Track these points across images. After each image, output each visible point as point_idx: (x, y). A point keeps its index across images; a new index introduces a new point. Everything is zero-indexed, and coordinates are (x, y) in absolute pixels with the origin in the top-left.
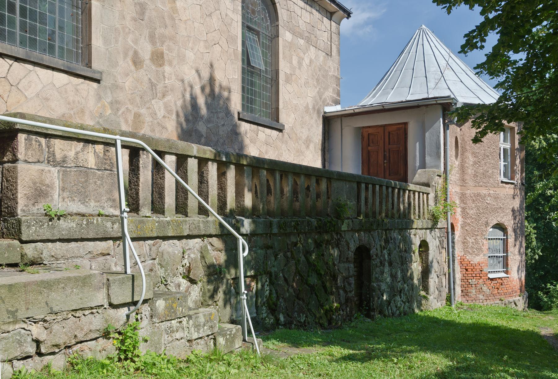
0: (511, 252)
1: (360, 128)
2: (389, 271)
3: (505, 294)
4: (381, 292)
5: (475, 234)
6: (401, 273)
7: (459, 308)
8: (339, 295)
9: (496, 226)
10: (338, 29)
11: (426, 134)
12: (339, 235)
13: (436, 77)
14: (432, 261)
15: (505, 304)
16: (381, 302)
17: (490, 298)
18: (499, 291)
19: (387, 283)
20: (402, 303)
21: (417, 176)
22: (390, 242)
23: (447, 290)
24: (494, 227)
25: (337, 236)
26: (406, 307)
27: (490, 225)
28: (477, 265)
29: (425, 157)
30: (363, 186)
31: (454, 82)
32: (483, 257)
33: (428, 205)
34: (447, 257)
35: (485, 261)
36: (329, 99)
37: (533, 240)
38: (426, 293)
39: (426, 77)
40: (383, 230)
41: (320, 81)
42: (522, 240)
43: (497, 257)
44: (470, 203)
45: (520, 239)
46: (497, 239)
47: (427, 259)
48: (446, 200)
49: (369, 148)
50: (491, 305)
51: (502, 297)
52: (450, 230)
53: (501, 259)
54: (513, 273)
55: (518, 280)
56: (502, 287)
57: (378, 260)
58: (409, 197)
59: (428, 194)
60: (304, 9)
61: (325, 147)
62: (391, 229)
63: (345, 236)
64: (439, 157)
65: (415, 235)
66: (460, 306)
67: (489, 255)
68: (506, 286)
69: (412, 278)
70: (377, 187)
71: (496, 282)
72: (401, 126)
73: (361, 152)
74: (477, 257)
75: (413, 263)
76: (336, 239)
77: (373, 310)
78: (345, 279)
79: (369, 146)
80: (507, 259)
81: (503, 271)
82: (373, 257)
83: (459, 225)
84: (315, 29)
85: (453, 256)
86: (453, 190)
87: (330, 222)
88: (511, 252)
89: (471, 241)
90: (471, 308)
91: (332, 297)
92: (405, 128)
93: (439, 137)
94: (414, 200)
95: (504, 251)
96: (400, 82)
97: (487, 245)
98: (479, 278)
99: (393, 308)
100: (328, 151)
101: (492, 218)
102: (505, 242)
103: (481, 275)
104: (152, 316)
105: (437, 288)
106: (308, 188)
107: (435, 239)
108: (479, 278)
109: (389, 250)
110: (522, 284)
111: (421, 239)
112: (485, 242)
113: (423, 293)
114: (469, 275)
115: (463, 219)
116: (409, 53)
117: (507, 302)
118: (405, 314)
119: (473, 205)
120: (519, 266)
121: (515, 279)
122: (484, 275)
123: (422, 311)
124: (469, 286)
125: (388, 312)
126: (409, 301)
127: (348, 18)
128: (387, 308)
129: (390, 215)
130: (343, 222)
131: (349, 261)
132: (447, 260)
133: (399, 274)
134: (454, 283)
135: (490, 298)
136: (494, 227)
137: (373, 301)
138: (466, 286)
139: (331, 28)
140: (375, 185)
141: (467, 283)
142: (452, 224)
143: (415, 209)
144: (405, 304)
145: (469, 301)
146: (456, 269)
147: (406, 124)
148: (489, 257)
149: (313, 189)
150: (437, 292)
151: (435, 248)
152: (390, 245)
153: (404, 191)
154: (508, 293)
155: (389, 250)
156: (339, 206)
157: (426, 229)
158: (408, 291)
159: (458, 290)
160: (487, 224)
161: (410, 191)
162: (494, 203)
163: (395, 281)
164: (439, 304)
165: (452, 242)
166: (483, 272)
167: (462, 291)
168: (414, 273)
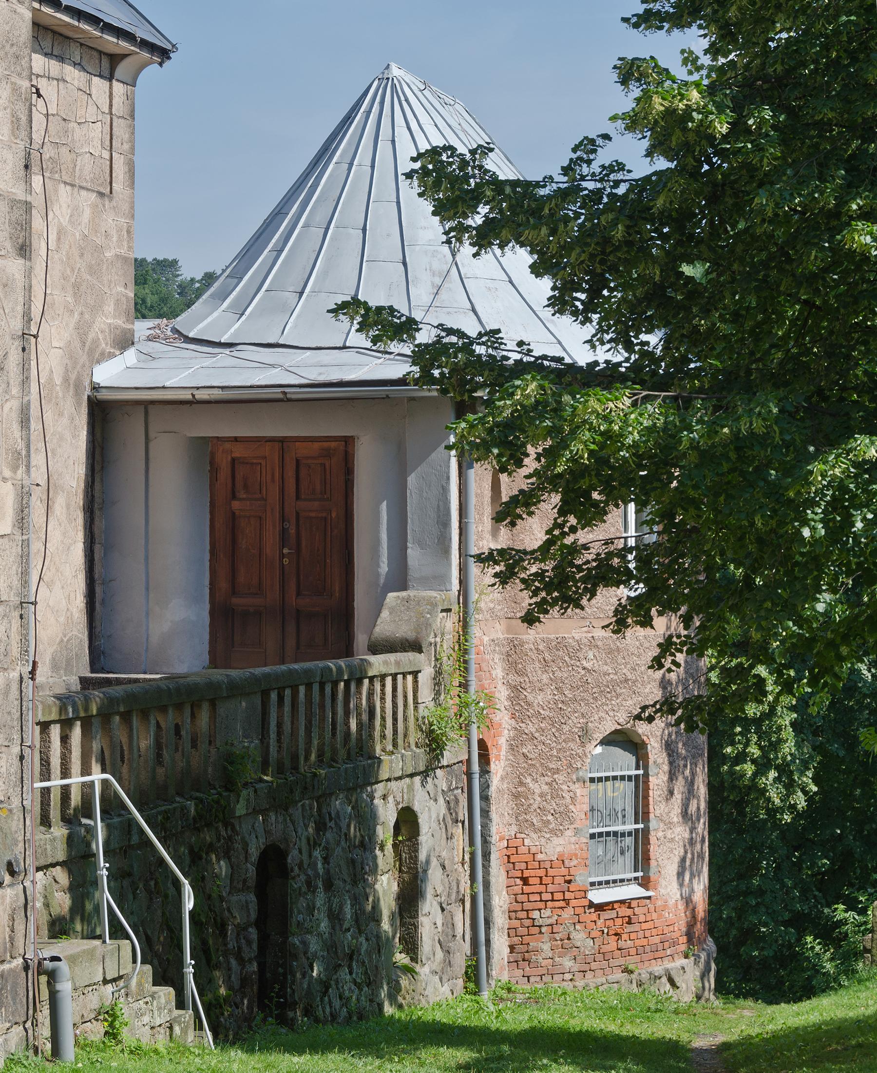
0: (660, 819)
1: (205, 440)
2: (325, 903)
3: (641, 950)
4: (308, 959)
5: (551, 766)
6: (352, 906)
7: (502, 999)
8: (229, 969)
9: (613, 737)
10: (130, 99)
11: (409, 479)
12: (229, 828)
13: (436, 265)
14: (428, 862)
15: (640, 984)
16: (309, 985)
17: (594, 965)
18: (621, 944)
19: (320, 935)
20: (353, 987)
21: (385, 614)
22: (329, 824)
23: (467, 948)
24: (607, 741)
25: (226, 830)
26: (363, 998)
27: (595, 736)
28: (557, 863)
29: (406, 548)
30: (274, 696)
31: (490, 284)
32: (573, 839)
33: (416, 703)
34: (467, 849)
35: (579, 852)
36: (105, 339)
37: (784, 735)
38: (412, 959)
39: (405, 264)
40: (312, 798)
41: (83, 288)
42: (693, 774)
43: (615, 834)
44: (535, 672)
45: (687, 772)
46: (615, 778)
47: (414, 858)
48: (464, 686)
49: (236, 505)
50: (597, 987)
51: (631, 962)
52: (476, 768)
53: (629, 841)
54: (663, 883)
55: (681, 906)
56: (630, 928)
57: (303, 878)
58: (371, 694)
59: (415, 674)
60: (44, 76)
61: (93, 496)
62: (331, 794)
63: (240, 827)
64: (447, 551)
65: (384, 797)
66: (504, 993)
67: (592, 831)
68: (644, 926)
69: (375, 916)
70: (302, 689)
71: (613, 914)
72: (333, 445)
73: (208, 516)
74: (556, 841)
75: (379, 877)
76: (224, 838)
77: (293, 1005)
78: (241, 929)
79: (234, 497)
80: (647, 842)
81: (636, 879)
82: (292, 870)
83: (503, 741)
84: (73, 125)
85: (486, 842)
86: (486, 639)
87: (218, 802)
88: (660, 819)
89: (537, 791)
90: (534, 999)
91: (217, 973)
92: (346, 452)
93: (445, 490)
94: (383, 699)
95: (636, 814)
96: (325, 273)
97: (587, 800)
98: (562, 904)
99: (333, 1001)
100: (101, 509)
101: (603, 715)
102: (641, 785)
103: (568, 895)
104: (127, 995)
105: (439, 941)
106: (177, 729)
107: (436, 800)
108: (562, 904)
109: (326, 848)
110: (694, 917)
111: (400, 807)
112: (579, 792)
113: (401, 958)
114: (533, 898)
115: (513, 722)
116: (351, 164)
117: (645, 976)
118: (361, 1018)
119: (545, 678)
120: (683, 860)
121: (671, 902)
122: (578, 895)
123: (400, 1007)
124: (535, 930)
125: (324, 1011)
126: (371, 982)
127: (161, 64)
128: (322, 1000)
129: (328, 755)
130: (239, 796)
131: (248, 888)
132: (467, 857)
133: (348, 910)
134: (488, 923)
135: (594, 965)
136: (607, 741)
137: (293, 982)
138: (523, 931)
139: (111, 106)
140: (297, 686)
141: (527, 922)
142: (482, 744)
143: (383, 726)
144: (361, 990)
145: (532, 979)
146: (493, 880)
147: (352, 438)
148: (592, 836)
149: (187, 733)
150: (440, 954)
151: (434, 825)
152: (329, 835)
153: (359, 682)
154: (648, 949)
155: (326, 848)
156: (229, 758)
157: (412, 776)
158: (369, 953)
159: (500, 944)
160: (585, 734)
161: (371, 679)
162: (606, 668)
163: (337, 928)
164: (445, 989)
165: (481, 798)
166: (572, 887)
167: (512, 948)
168: (382, 902)
